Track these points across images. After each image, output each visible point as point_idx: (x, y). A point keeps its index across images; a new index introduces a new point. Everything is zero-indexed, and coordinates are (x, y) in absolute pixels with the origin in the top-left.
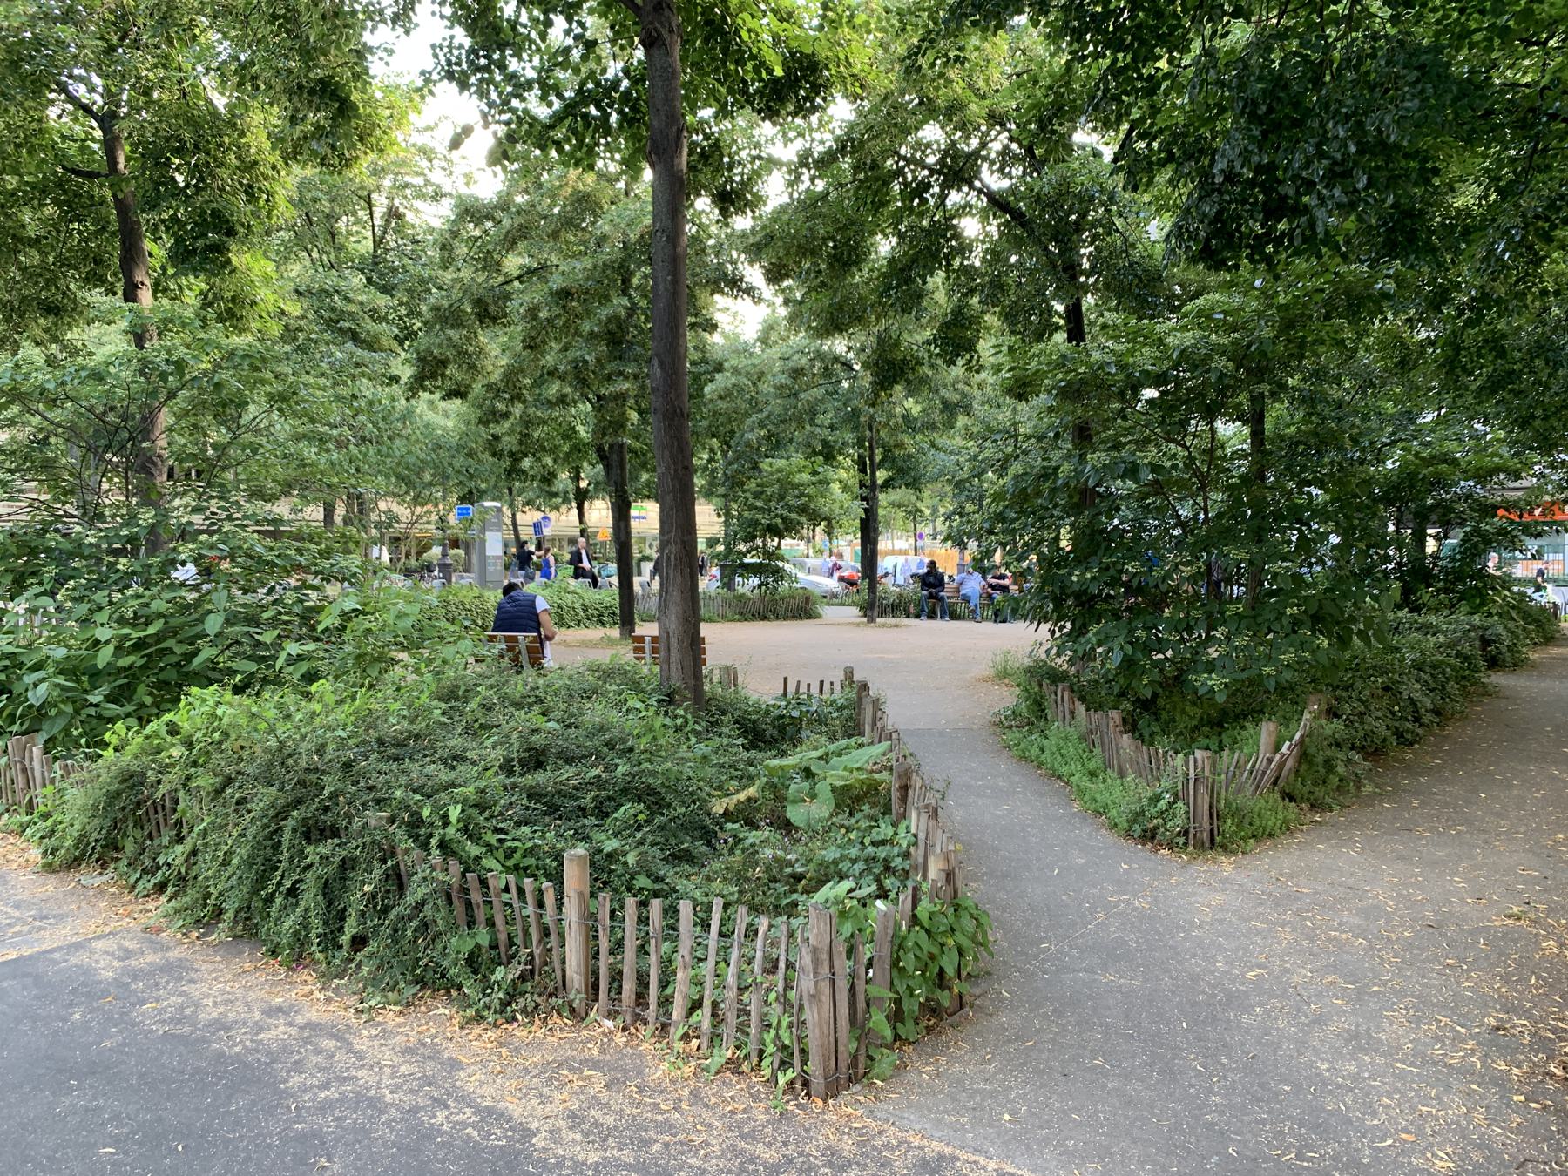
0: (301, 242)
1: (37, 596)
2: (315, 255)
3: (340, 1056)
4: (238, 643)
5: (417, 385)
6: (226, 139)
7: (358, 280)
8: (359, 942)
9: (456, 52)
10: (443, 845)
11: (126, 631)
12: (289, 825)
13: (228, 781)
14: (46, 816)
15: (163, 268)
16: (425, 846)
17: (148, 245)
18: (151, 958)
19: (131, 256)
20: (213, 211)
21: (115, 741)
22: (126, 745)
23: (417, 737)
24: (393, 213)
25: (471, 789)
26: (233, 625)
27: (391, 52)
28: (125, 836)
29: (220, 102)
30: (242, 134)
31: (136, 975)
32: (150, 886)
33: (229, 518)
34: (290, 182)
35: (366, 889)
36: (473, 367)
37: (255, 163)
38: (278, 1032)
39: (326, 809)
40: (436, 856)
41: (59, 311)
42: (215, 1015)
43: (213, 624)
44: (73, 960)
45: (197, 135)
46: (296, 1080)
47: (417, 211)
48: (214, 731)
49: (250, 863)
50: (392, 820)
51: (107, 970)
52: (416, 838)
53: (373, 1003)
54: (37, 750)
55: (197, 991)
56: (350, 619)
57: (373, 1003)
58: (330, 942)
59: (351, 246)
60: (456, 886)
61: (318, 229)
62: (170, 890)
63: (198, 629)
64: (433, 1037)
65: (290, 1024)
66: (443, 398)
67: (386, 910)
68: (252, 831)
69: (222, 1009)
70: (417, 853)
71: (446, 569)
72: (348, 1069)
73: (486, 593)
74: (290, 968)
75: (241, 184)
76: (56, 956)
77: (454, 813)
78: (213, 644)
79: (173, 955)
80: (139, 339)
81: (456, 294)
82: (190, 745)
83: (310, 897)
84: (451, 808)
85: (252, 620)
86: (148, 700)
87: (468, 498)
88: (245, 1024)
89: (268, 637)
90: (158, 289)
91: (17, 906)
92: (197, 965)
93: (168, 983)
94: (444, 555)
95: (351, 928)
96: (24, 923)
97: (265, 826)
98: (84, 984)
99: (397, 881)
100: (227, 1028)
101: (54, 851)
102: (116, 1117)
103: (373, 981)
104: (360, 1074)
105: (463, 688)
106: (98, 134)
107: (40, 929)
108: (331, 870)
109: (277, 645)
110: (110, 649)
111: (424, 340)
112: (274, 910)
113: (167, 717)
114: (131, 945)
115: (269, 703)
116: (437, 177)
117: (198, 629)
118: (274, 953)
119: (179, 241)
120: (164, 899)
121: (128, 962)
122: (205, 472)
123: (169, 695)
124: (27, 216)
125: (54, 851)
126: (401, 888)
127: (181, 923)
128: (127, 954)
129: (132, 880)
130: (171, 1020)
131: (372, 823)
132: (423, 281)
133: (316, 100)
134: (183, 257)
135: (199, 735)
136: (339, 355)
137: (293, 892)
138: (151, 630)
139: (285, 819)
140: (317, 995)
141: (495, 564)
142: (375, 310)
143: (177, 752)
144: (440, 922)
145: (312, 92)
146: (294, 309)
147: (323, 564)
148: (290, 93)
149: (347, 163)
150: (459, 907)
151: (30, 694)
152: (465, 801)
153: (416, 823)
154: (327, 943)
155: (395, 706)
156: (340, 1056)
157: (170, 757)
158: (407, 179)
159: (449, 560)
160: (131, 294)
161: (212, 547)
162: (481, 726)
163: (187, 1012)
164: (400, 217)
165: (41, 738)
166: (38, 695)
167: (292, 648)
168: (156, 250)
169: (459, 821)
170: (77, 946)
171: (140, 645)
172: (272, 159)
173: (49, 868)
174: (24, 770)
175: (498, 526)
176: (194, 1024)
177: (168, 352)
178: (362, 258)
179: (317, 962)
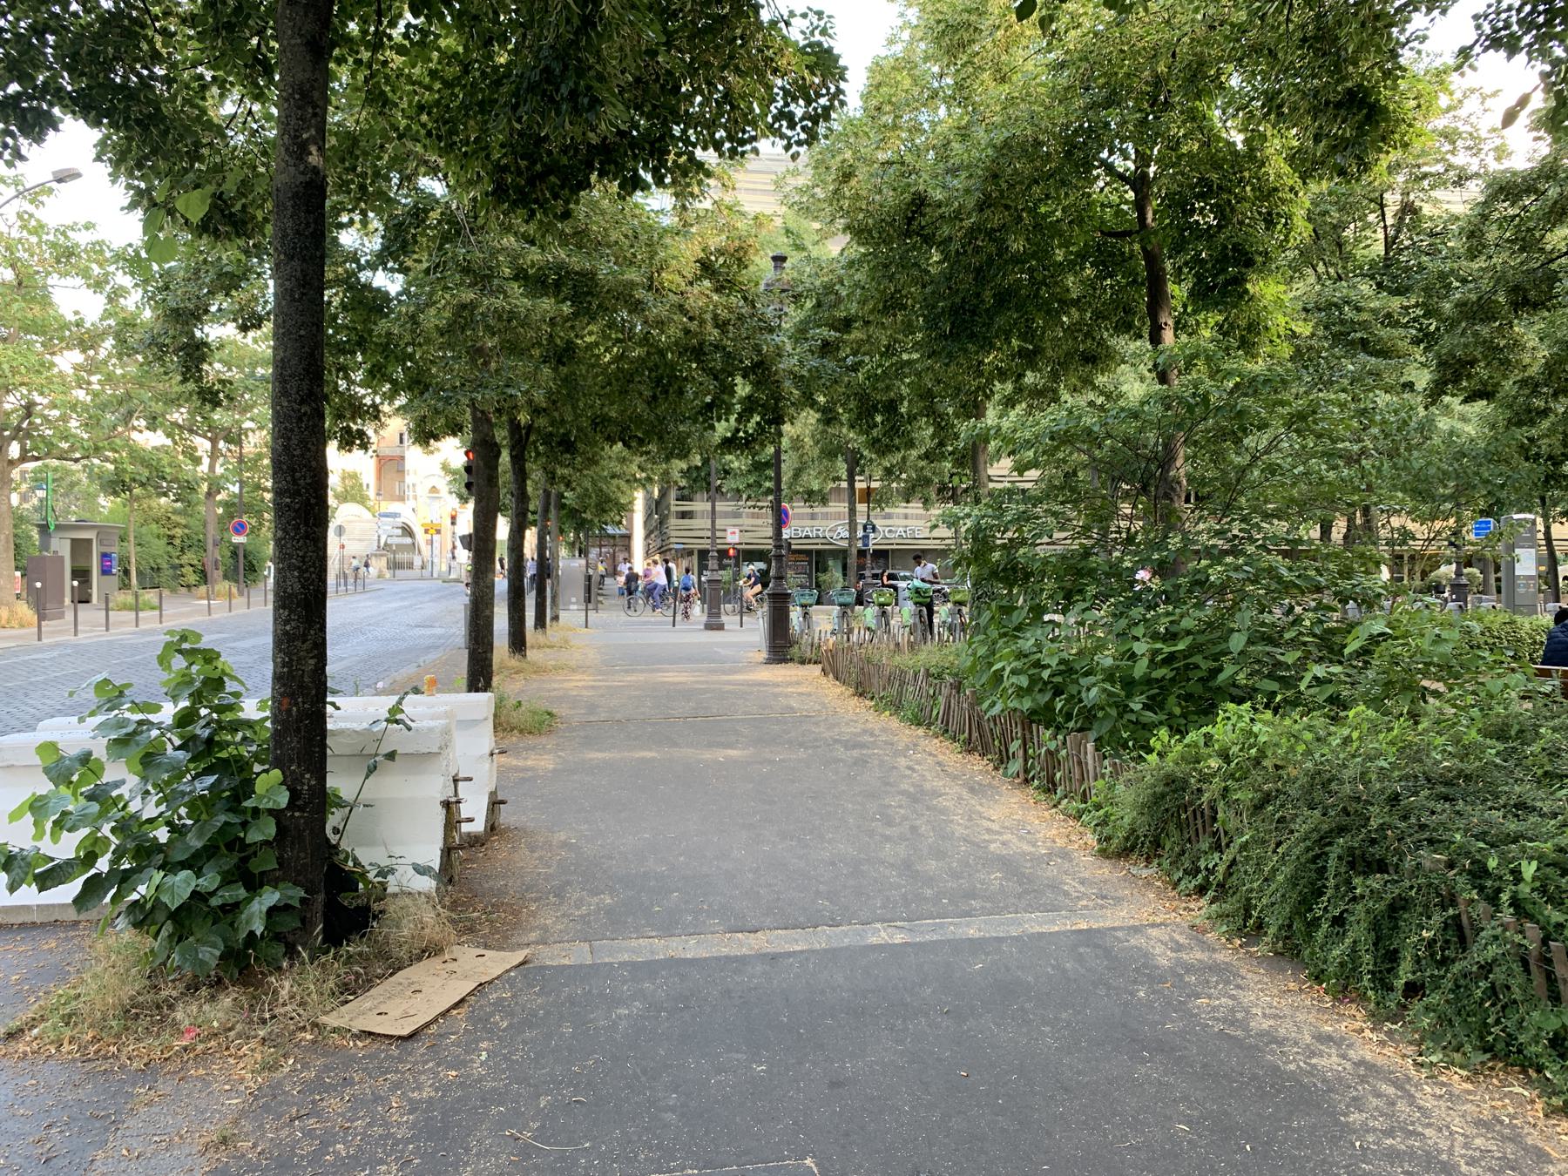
0: (1306, 257)
1: (1084, 611)
2: (1321, 268)
3: (1401, 1105)
4: (1258, 662)
5: (1436, 393)
6: (1246, 174)
7: (1366, 288)
8: (1412, 990)
9: (1504, 16)
10: (1515, 902)
11: (1159, 646)
12: (1334, 852)
13: (1267, 799)
14: (1098, 807)
15: (1185, 306)
16: (1493, 899)
17: (1172, 288)
18: (1199, 955)
19: (1157, 299)
20: (1234, 246)
21: (1158, 746)
22: (1167, 750)
23: (1468, 778)
24: (1408, 209)
25: (1549, 845)
26: (1253, 643)
27: (1425, 38)
28: (1169, 834)
29: (1238, 139)
30: (1263, 164)
31: (1189, 968)
32: (1191, 886)
33: (1252, 540)
34: (1303, 201)
35: (1425, 933)
36: (1506, 363)
37: (1276, 190)
38: (1330, 1061)
39: (1373, 842)
40: (1507, 915)
41: (1097, 358)
42: (1265, 1026)
43: (1237, 642)
44: (1133, 942)
45: (1222, 178)
46: (1355, 1117)
47: (1436, 202)
48: (1251, 747)
49: (1293, 881)
50: (1451, 865)
51: (1164, 958)
52: (1481, 889)
53: (1434, 1059)
54: (1090, 746)
55: (1247, 998)
56: (1378, 643)
57: (1434, 1059)
58: (1383, 983)
59: (1359, 253)
60: (1535, 953)
61: (1328, 242)
62: (1211, 894)
63: (1223, 646)
64: (1512, 1117)
65: (1344, 1057)
66: (1465, 401)
67: (1445, 962)
68: (1297, 851)
69: (1272, 1022)
70: (1482, 907)
71: (1460, 590)
72: (1413, 1123)
73: (1519, 619)
74: (1335, 999)
75: (1260, 213)
76: (1120, 934)
77: (1529, 870)
78: (1235, 662)
79: (1222, 957)
80: (1163, 378)
81: (1486, 285)
82: (1226, 757)
83: (1358, 930)
84: (1524, 863)
85: (1269, 640)
86: (1177, 711)
87: (1494, 509)
88: (1296, 1043)
89: (1291, 657)
90: (1179, 326)
91: (1082, 883)
92: (1243, 972)
93: (1217, 983)
94: (1459, 574)
95: (1405, 973)
96: (1089, 899)
97: (1308, 849)
98: (1145, 966)
99: (1459, 934)
100: (1280, 1043)
101: (1108, 839)
102: (1185, 1098)
103: (1433, 1035)
104: (1428, 1132)
105: (1516, 727)
106: (1131, 195)
107: (1102, 907)
108: (1381, 906)
109: (1301, 666)
110: (1145, 662)
111: (1446, 343)
112: (1320, 935)
113: (1204, 730)
114: (1182, 940)
115: (1294, 721)
116: (1460, 159)
117: (1223, 646)
118: (1318, 978)
119: (1199, 278)
120: (1204, 902)
121: (1180, 955)
122: (1219, 496)
123: (1204, 707)
124: (1070, 281)
125: (1108, 839)
126: (1463, 943)
127: (1225, 928)
128: (1178, 948)
129: (1176, 877)
130: (1225, 1020)
131: (1427, 864)
132: (1442, 276)
133: (1343, 112)
134: (1203, 296)
135: (1235, 749)
136: (1351, 367)
137: (1339, 921)
138: (1181, 646)
139: (1330, 844)
140: (1367, 1033)
141: (1528, 586)
142: (1389, 316)
143: (1214, 763)
144: (1515, 989)
145: (1338, 105)
146: (1304, 329)
147: (1345, 584)
148: (1315, 112)
149: (1365, 167)
150: (1538, 978)
151: (1083, 695)
152: (1540, 858)
153: (1479, 873)
154: (1376, 977)
155: (1440, 740)
156: (1401, 1105)
157: (1209, 767)
158: (1425, 169)
159: (1464, 581)
160: (1156, 339)
161: (1237, 569)
162: (1546, 773)
163: (1239, 1016)
164: (1415, 211)
165: (1092, 735)
166: (1093, 695)
167: (1319, 670)
168: (1178, 291)
169: (1534, 879)
170: (1136, 930)
171: (1170, 659)
172: (1291, 182)
173: (1103, 853)
174: (1080, 763)
175: (1532, 543)
176: (1247, 1029)
177: (1196, 387)
178: (1373, 264)
179: (1369, 1000)
